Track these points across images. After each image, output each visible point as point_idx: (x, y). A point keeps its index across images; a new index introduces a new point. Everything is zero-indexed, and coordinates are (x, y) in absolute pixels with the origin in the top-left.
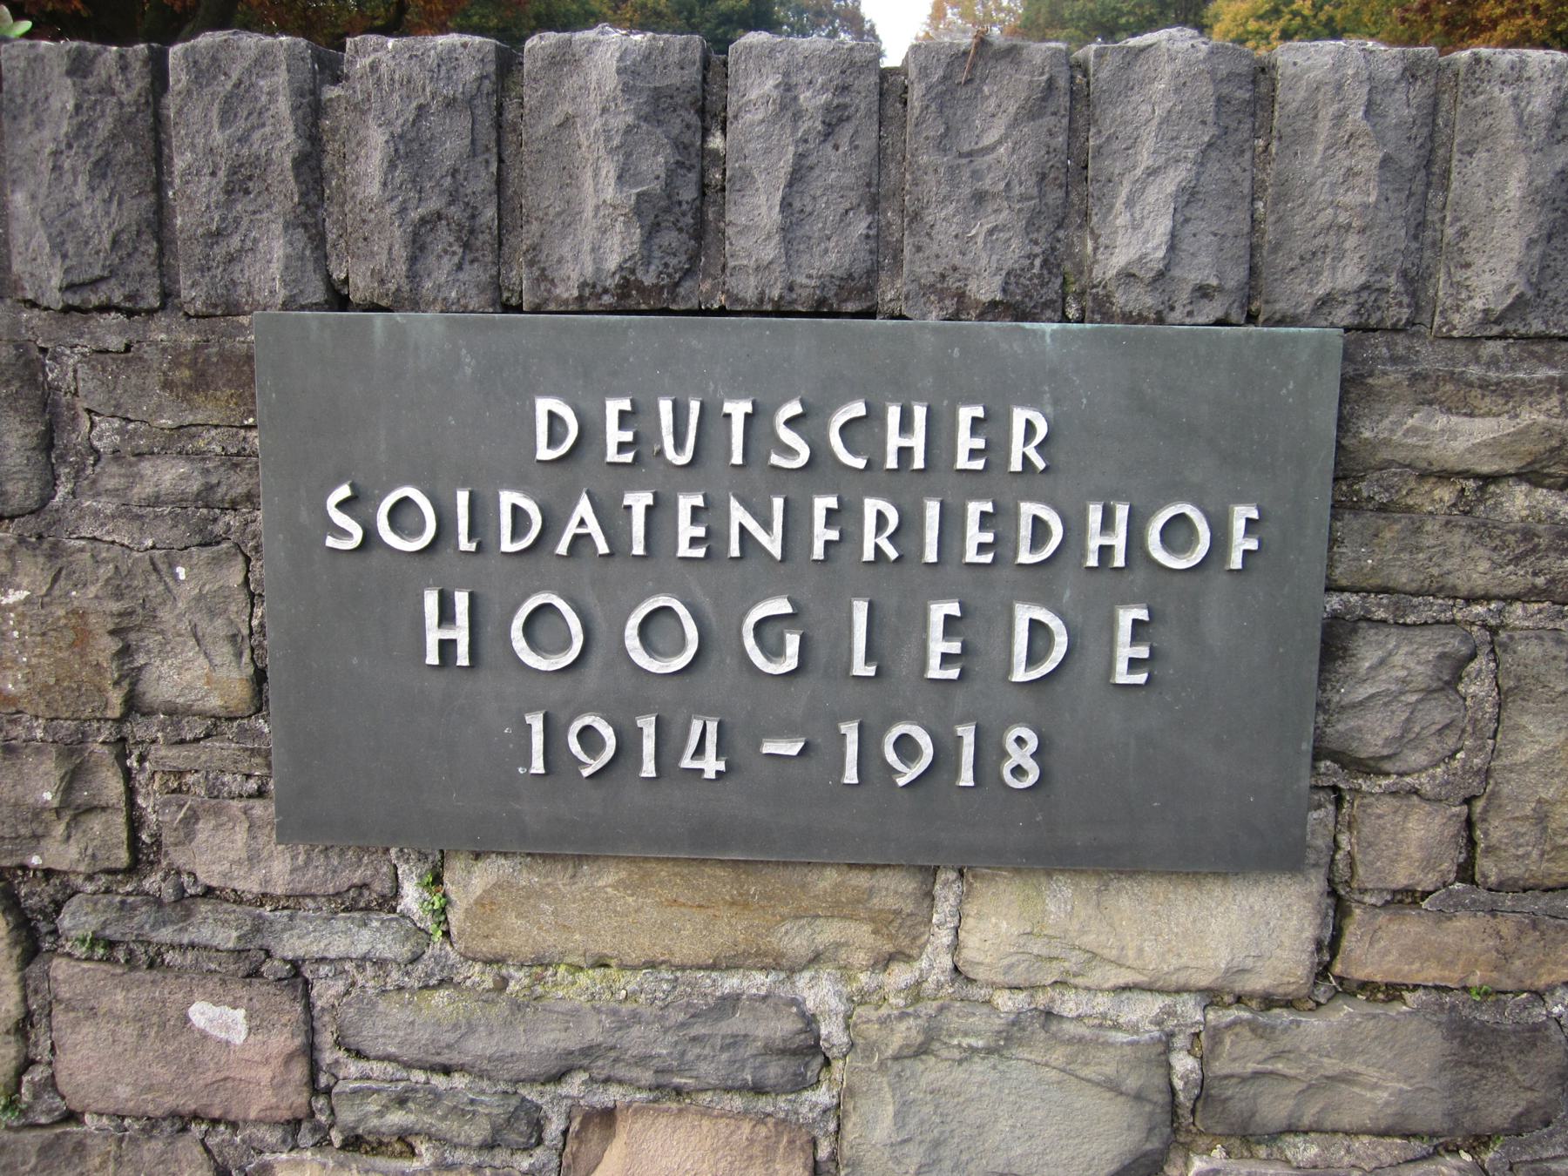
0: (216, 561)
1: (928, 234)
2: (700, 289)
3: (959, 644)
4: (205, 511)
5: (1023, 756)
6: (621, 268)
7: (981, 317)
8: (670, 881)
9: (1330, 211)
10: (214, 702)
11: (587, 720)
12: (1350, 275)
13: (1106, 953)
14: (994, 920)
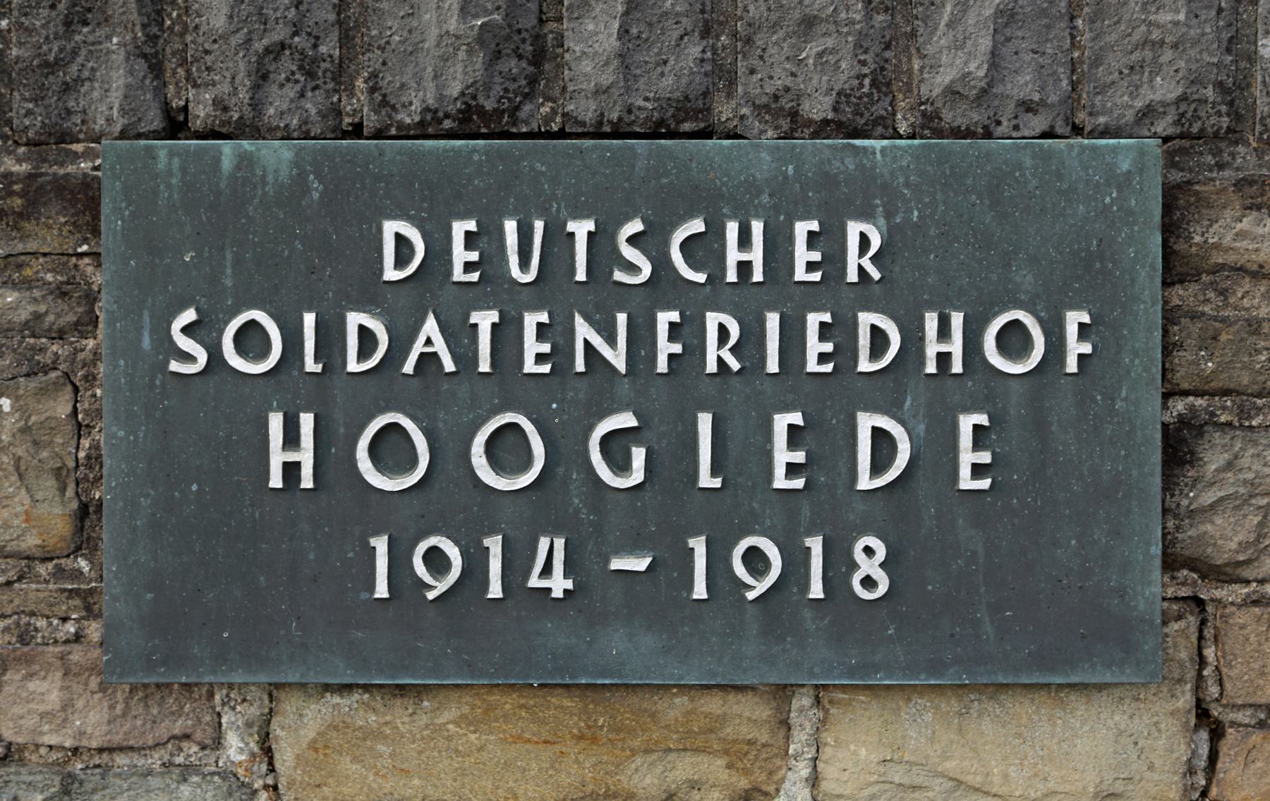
0: (43, 392)
1: (761, 57)
2: (538, 112)
3: (804, 453)
4: (32, 341)
5: (872, 566)
6: (463, 94)
7: (815, 135)
8: (515, 714)
9: (1143, 28)
10: (31, 541)
11: (433, 541)
12: (1164, 89)
13: (969, 779)
14: (852, 747)
